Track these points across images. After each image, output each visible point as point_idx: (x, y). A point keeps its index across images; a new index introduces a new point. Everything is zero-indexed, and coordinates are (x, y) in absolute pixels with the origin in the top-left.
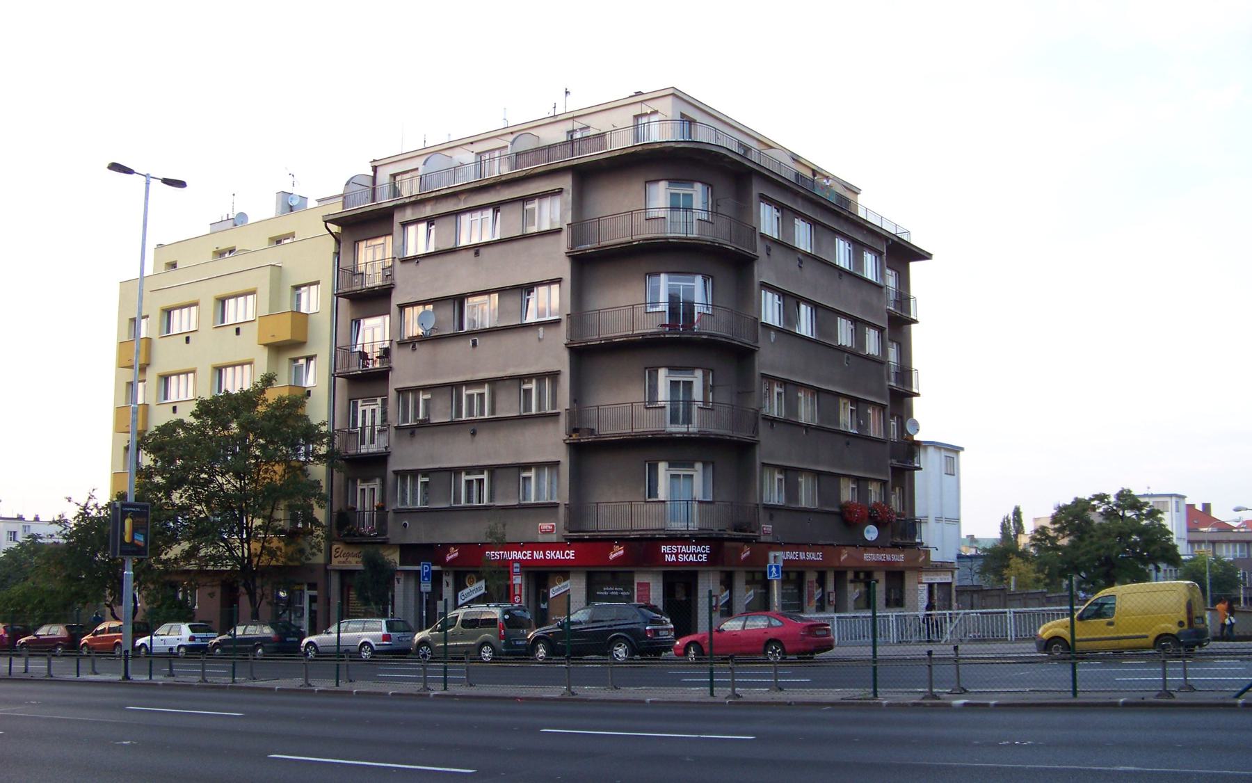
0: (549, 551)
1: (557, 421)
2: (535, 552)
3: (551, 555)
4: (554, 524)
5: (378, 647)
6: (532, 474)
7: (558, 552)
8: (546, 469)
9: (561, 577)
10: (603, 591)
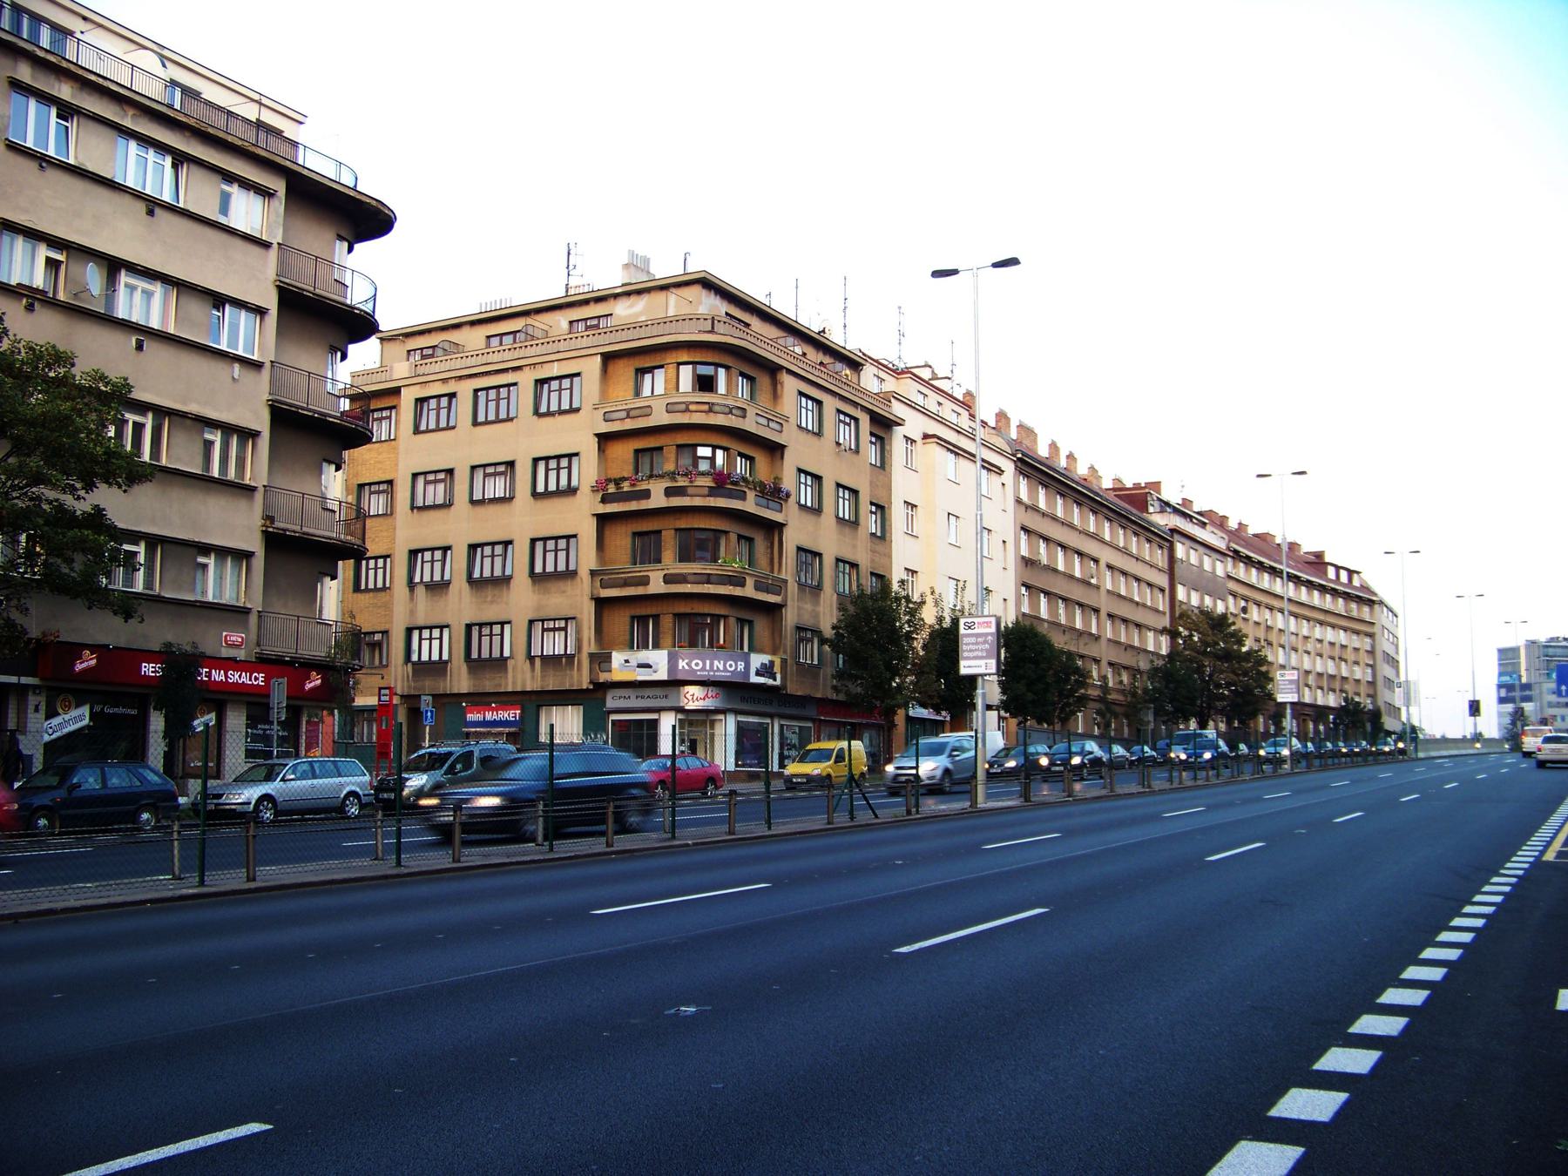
0: (231, 672)
1: (251, 498)
2: (213, 671)
3: (234, 677)
4: (243, 635)
5: (367, 798)
6: (211, 561)
7: (244, 674)
8: (229, 559)
9: (205, 708)
10: (257, 729)
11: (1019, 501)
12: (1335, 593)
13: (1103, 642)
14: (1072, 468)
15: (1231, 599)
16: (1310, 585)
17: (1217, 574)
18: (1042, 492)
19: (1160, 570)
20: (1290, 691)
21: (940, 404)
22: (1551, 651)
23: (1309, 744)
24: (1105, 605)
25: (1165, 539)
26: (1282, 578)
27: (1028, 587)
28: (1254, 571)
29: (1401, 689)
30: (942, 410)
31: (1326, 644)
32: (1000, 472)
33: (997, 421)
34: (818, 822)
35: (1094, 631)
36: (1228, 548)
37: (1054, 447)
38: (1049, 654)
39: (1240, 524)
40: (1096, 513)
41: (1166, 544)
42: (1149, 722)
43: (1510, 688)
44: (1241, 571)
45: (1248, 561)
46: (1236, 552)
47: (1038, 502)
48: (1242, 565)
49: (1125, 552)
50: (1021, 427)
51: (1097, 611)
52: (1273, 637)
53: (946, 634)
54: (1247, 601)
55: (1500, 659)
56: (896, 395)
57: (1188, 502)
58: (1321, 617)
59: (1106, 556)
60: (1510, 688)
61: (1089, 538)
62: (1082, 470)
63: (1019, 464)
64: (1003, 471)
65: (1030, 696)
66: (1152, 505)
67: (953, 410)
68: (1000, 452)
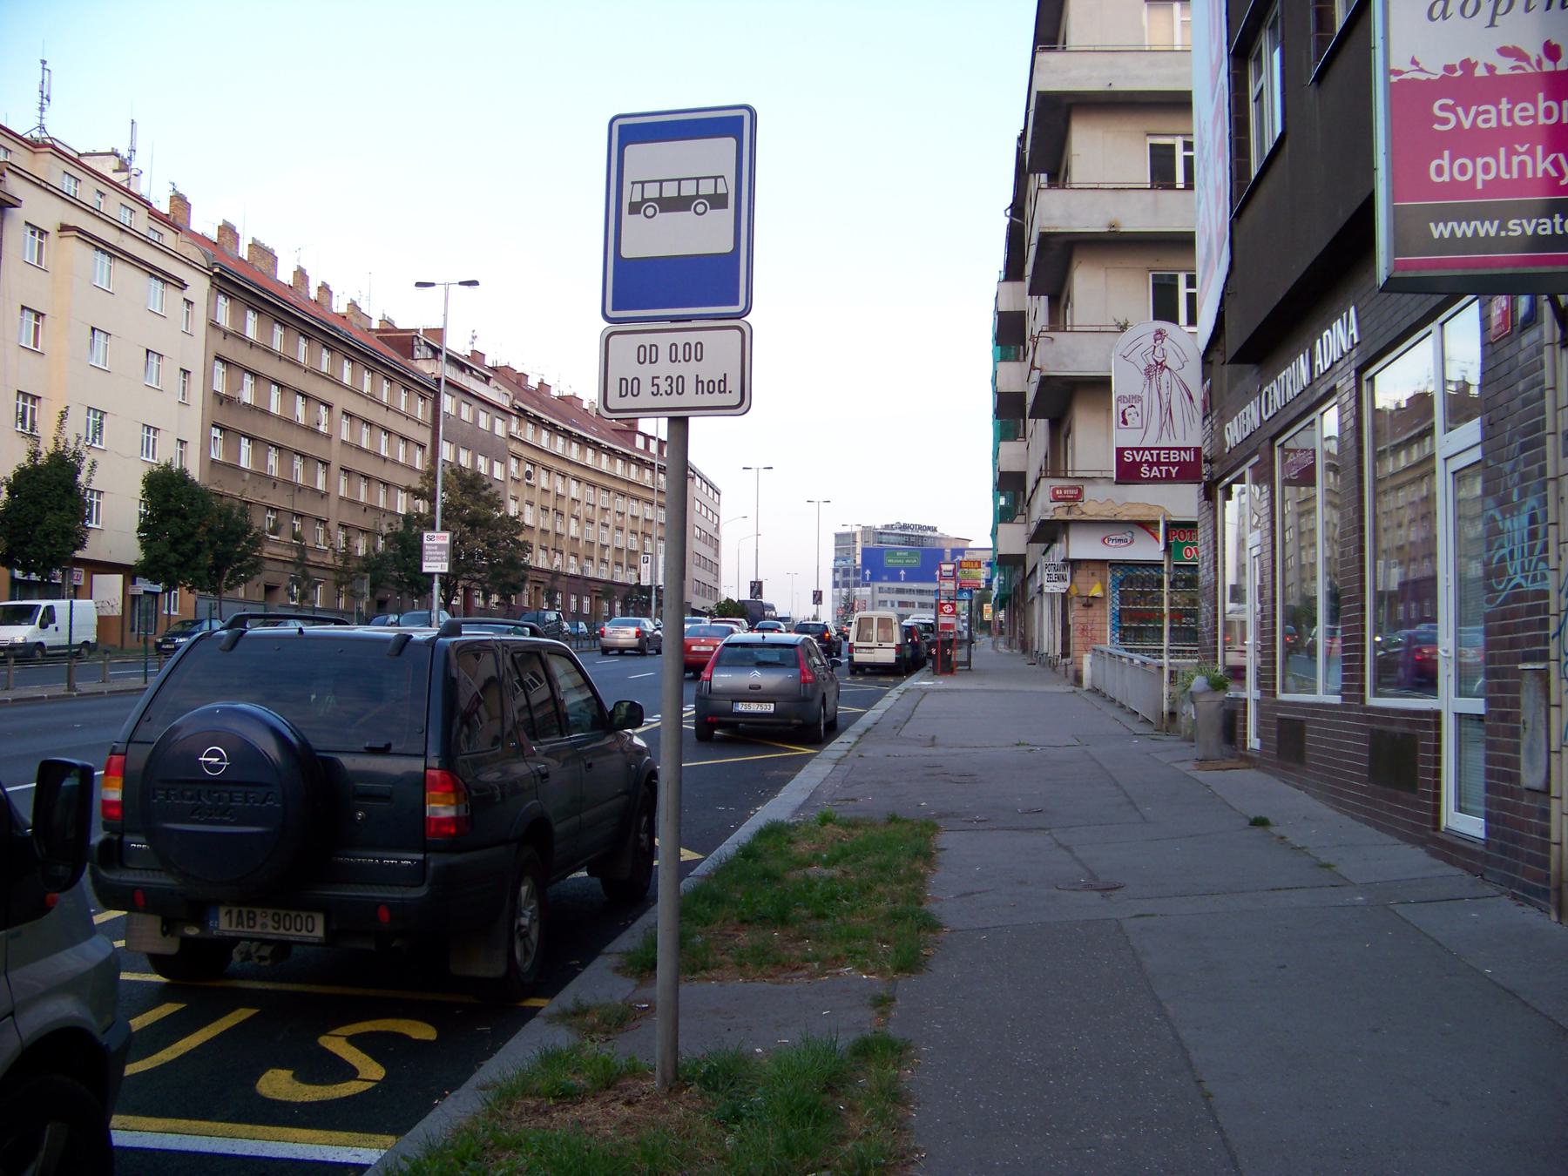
11: (213, 325)
12: (641, 463)
13: (333, 500)
14: (324, 301)
15: (513, 462)
16: (611, 452)
17: (497, 433)
18: (251, 318)
19: (419, 423)
20: (439, 558)
21: (102, 195)
22: (885, 538)
23: (582, 624)
24: (337, 458)
25: (429, 390)
26: (653, 470)
27: (223, 429)
28: (545, 434)
29: (649, 564)
30: (105, 202)
31: (627, 517)
32: (182, 285)
33: (219, 236)
34: (60, 689)
35: (320, 486)
36: (513, 406)
37: (301, 274)
38: (201, 506)
39: (541, 383)
40: (309, 338)
41: (430, 394)
42: (363, 595)
43: (846, 573)
44: (528, 433)
45: (538, 422)
46: (521, 410)
47: (244, 328)
48: (530, 425)
49: (372, 399)
50: (255, 246)
51: (326, 464)
52: (565, 507)
53: (37, 474)
54: (534, 466)
55: (836, 545)
56: (11, 167)
57: (478, 355)
58: (623, 488)
59: (342, 401)
60: (846, 573)
61: (317, 378)
62: (339, 306)
63: (217, 281)
64: (186, 285)
65: (173, 557)
66: (419, 350)
67: (122, 204)
68: (189, 263)
